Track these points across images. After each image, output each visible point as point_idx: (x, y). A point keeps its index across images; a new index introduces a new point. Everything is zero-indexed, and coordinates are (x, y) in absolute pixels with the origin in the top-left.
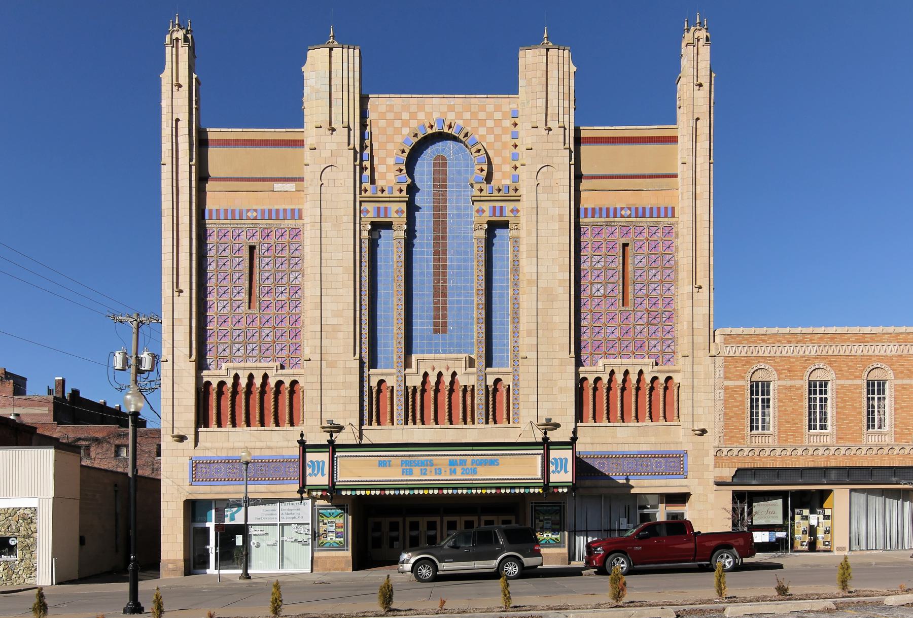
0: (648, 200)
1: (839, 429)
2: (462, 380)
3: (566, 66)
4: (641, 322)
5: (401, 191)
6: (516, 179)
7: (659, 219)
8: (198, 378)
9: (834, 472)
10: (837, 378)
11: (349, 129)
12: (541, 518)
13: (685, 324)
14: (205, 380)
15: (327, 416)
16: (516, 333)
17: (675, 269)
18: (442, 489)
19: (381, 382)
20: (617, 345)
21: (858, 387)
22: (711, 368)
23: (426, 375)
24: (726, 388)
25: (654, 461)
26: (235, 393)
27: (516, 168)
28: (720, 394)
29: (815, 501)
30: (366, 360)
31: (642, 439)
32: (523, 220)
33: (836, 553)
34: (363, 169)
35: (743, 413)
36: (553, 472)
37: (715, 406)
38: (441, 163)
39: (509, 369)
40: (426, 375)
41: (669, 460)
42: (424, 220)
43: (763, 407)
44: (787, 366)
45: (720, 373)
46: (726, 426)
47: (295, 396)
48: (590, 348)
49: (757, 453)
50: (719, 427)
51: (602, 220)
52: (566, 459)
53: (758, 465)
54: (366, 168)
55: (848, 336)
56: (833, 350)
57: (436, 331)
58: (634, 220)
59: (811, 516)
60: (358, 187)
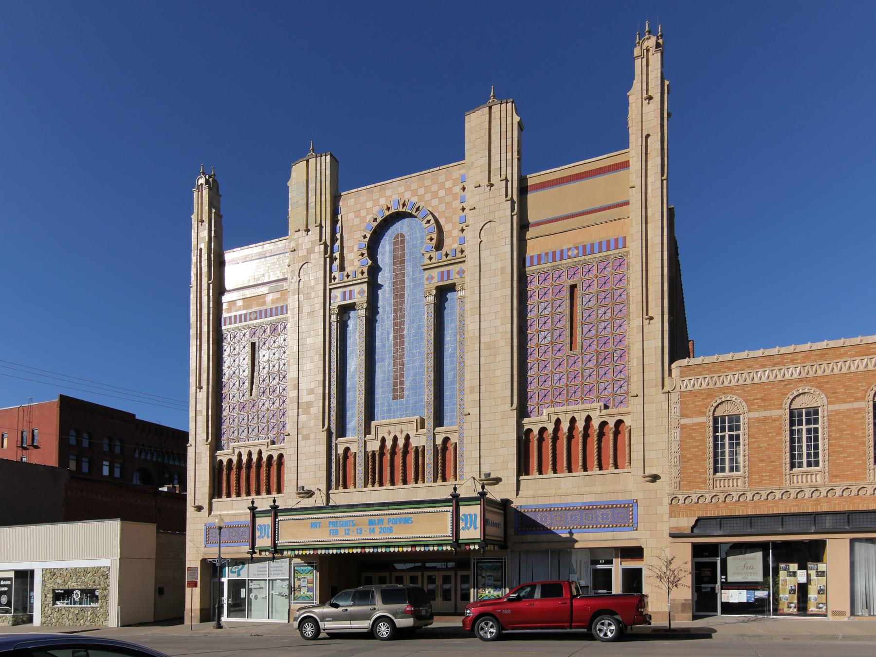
0: (597, 234)
1: (832, 464)
2: (414, 442)
3: (509, 119)
4: (591, 364)
5: (362, 273)
6: (463, 241)
7: (609, 253)
8: (519, 426)
9: (828, 517)
10: (829, 403)
11: (507, 181)
12: (484, 574)
13: (635, 360)
14: (526, 427)
15: (485, 469)
16: (462, 391)
17: (626, 304)
18: (414, 546)
19: (347, 450)
20: (565, 392)
21: (860, 410)
22: (665, 405)
23: (383, 440)
24: (683, 427)
25: (599, 512)
26: (555, 438)
27: (463, 230)
28: (676, 434)
29: (811, 553)
30: (334, 430)
31: (587, 489)
32: (467, 279)
33: (831, 618)
34: (333, 259)
35: (704, 453)
36: (463, 528)
37: (669, 448)
38: (400, 240)
39: (456, 427)
40: (383, 440)
41: (616, 511)
42: (385, 297)
43: (731, 445)
44: (762, 395)
45: (675, 411)
46: (682, 470)
47: (619, 437)
48: (537, 398)
49: (722, 499)
50: (675, 472)
51: (549, 265)
52: (476, 515)
53: (724, 513)
54: (336, 259)
55: (846, 349)
56: (824, 369)
57: (395, 398)
58: (582, 258)
59: (799, 572)
60: (328, 277)
